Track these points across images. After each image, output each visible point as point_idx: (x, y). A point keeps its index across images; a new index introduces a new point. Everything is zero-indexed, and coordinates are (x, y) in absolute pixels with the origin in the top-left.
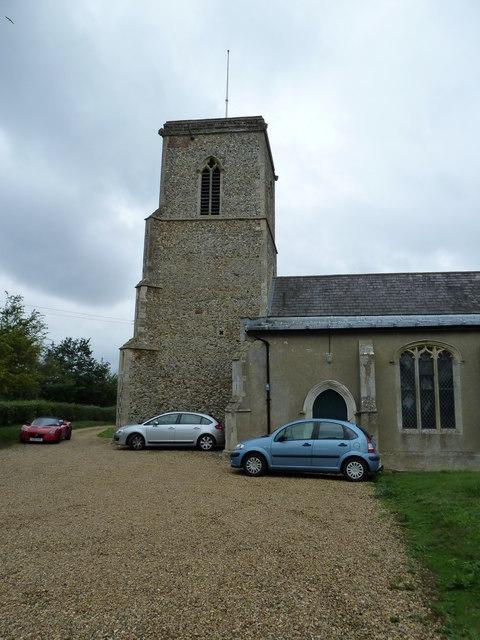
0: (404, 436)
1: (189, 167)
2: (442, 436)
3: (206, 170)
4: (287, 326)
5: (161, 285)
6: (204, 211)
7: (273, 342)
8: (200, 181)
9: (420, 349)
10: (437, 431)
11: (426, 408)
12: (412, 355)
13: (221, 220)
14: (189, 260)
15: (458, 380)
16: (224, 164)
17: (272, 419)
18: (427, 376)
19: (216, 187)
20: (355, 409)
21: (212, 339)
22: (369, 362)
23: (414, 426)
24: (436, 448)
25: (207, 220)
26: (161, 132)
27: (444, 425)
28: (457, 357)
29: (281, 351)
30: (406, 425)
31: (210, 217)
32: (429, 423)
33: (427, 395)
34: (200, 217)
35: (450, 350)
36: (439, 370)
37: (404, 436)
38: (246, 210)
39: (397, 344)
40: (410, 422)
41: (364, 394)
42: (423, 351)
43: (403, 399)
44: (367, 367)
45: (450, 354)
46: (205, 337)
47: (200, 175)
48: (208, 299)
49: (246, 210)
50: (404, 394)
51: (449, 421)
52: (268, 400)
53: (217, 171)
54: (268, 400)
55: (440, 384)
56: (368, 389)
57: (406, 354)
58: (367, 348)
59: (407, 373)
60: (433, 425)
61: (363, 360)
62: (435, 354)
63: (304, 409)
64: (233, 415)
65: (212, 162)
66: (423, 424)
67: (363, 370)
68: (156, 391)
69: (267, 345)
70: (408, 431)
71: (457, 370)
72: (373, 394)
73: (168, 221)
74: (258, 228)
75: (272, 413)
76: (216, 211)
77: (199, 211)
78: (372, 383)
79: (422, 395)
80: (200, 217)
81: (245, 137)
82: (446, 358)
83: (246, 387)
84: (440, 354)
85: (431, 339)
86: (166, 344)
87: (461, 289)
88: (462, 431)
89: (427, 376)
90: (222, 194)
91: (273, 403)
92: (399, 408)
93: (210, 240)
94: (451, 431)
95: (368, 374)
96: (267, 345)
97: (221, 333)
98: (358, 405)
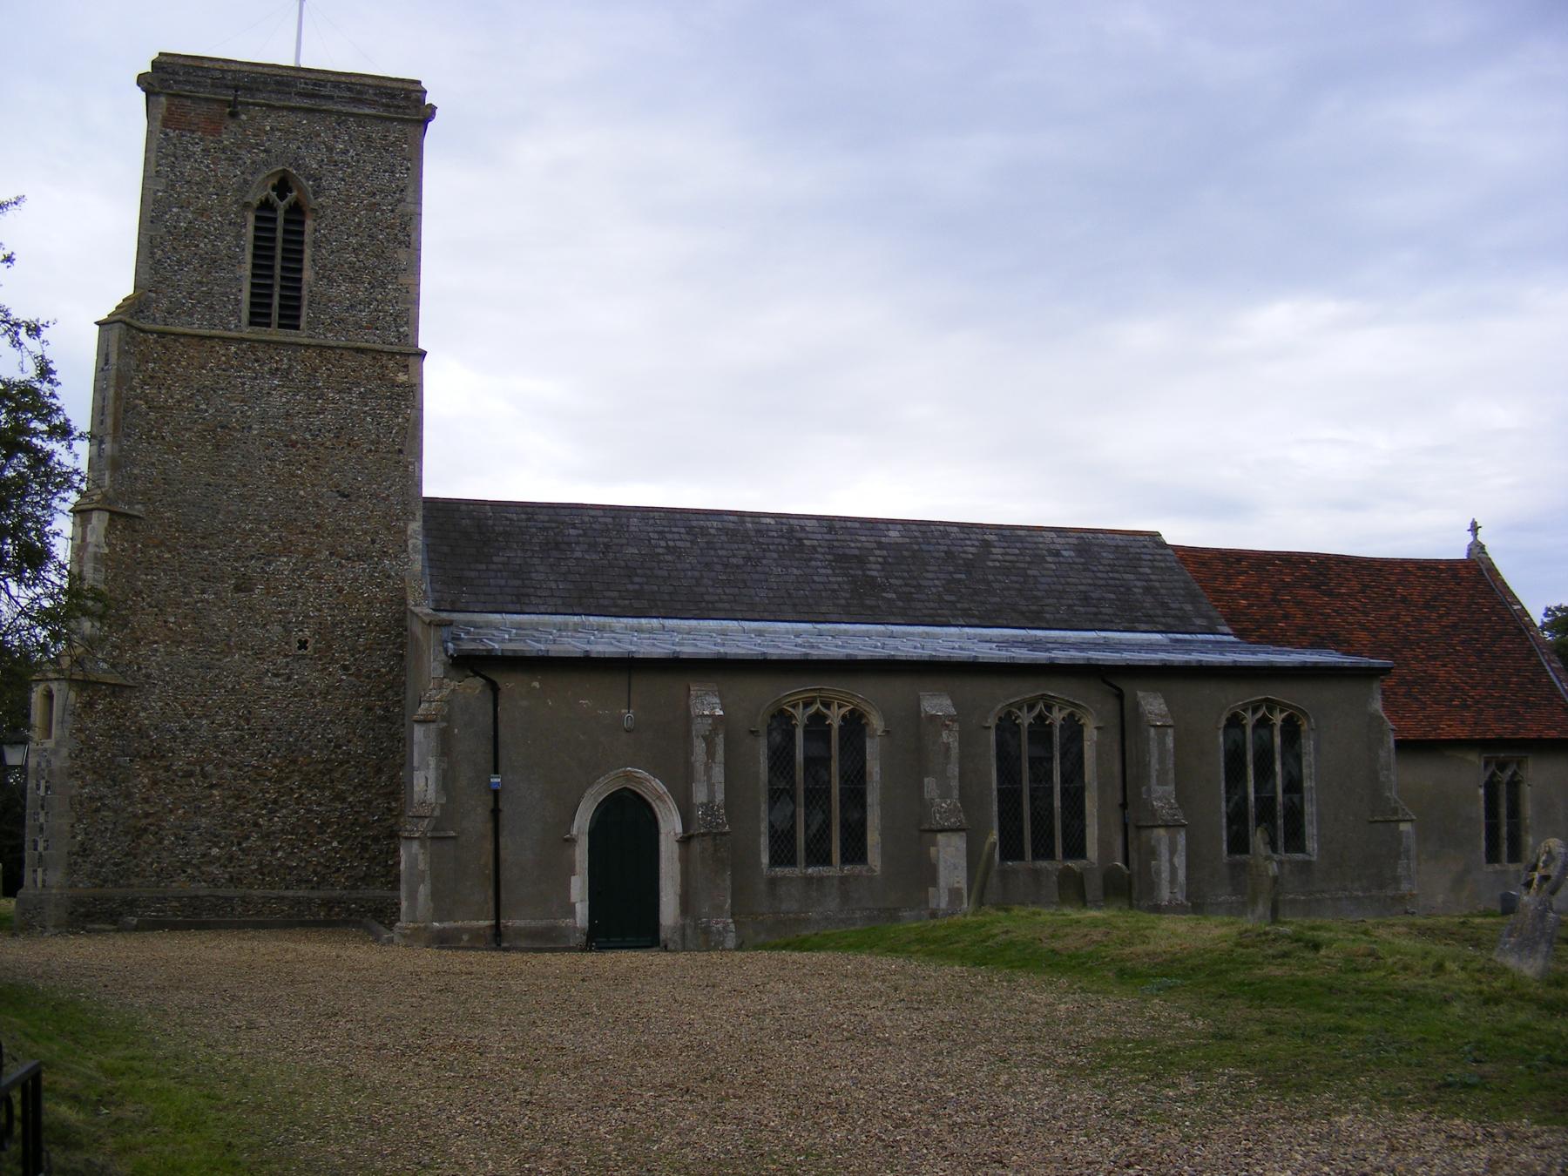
0: (773, 882)
1: (221, 191)
2: (844, 880)
3: (266, 205)
4: (534, 647)
5: (138, 509)
6: (259, 316)
7: (509, 683)
8: (249, 231)
9: (807, 705)
10: (835, 870)
11: (814, 828)
12: (792, 716)
13: (308, 346)
14: (217, 447)
15: (874, 767)
16: (316, 194)
17: (503, 853)
18: (817, 763)
19: (294, 255)
20: (679, 829)
21: (281, 660)
22: (714, 731)
23: (792, 862)
24: (832, 904)
25: (268, 343)
26: (142, 80)
27: (846, 860)
28: (876, 723)
29: (524, 703)
30: (775, 861)
31: (275, 334)
32: (819, 856)
33: (817, 796)
34: (248, 332)
35: (864, 707)
36: (841, 749)
37: (1004, 874)
38: (372, 325)
39: (762, 694)
40: (782, 852)
41: (700, 795)
42: (812, 710)
43: (771, 809)
44: (709, 741)
45: (862, 716)
46: (259, 655)
47: (251, 218)
48: (269, 556)
49: (372, 325)
50: (775, 796)
51: (855, 851)
52: (496, 812)
53: (297, 213)
54: (496, 812)
55: (841, 777)
56: (709, 787)
57: (782, 718)
58: (708, 704)
59: (781, 759)
60: (826, 860)
61: (700, 728)
62: (835, 717)
63: (574, 831)
64: (423, 846)
65: (283, 185)
66: (843, 855)
67: (700, 747)
68: (129, 796)
69: (494, 688)
70: (779, 871)
71: (872, 748)
72: (720, 797)
73: (162, 334)
74: (402, 378)
75: (504, 840)
76: (290, 319)
77: (245, 315)
78: (718, 773)
79: (806, 798)
80: (248, 332)
81: (376, 131)
82: (855, 724)
83: (447, 781)
84: (844, 717)
85: (829, 686)
86: (155, 673)
87: (861, 560)
88: (878, 869)
89: (817, 763)
90: (308, 275)
91: (504, 817)
92: (764, 827)
93: (277, 399)
94: (858, 868)
95: (710, 753)
96: (494, 688)
97: (303, 645)
98: (686, 821)
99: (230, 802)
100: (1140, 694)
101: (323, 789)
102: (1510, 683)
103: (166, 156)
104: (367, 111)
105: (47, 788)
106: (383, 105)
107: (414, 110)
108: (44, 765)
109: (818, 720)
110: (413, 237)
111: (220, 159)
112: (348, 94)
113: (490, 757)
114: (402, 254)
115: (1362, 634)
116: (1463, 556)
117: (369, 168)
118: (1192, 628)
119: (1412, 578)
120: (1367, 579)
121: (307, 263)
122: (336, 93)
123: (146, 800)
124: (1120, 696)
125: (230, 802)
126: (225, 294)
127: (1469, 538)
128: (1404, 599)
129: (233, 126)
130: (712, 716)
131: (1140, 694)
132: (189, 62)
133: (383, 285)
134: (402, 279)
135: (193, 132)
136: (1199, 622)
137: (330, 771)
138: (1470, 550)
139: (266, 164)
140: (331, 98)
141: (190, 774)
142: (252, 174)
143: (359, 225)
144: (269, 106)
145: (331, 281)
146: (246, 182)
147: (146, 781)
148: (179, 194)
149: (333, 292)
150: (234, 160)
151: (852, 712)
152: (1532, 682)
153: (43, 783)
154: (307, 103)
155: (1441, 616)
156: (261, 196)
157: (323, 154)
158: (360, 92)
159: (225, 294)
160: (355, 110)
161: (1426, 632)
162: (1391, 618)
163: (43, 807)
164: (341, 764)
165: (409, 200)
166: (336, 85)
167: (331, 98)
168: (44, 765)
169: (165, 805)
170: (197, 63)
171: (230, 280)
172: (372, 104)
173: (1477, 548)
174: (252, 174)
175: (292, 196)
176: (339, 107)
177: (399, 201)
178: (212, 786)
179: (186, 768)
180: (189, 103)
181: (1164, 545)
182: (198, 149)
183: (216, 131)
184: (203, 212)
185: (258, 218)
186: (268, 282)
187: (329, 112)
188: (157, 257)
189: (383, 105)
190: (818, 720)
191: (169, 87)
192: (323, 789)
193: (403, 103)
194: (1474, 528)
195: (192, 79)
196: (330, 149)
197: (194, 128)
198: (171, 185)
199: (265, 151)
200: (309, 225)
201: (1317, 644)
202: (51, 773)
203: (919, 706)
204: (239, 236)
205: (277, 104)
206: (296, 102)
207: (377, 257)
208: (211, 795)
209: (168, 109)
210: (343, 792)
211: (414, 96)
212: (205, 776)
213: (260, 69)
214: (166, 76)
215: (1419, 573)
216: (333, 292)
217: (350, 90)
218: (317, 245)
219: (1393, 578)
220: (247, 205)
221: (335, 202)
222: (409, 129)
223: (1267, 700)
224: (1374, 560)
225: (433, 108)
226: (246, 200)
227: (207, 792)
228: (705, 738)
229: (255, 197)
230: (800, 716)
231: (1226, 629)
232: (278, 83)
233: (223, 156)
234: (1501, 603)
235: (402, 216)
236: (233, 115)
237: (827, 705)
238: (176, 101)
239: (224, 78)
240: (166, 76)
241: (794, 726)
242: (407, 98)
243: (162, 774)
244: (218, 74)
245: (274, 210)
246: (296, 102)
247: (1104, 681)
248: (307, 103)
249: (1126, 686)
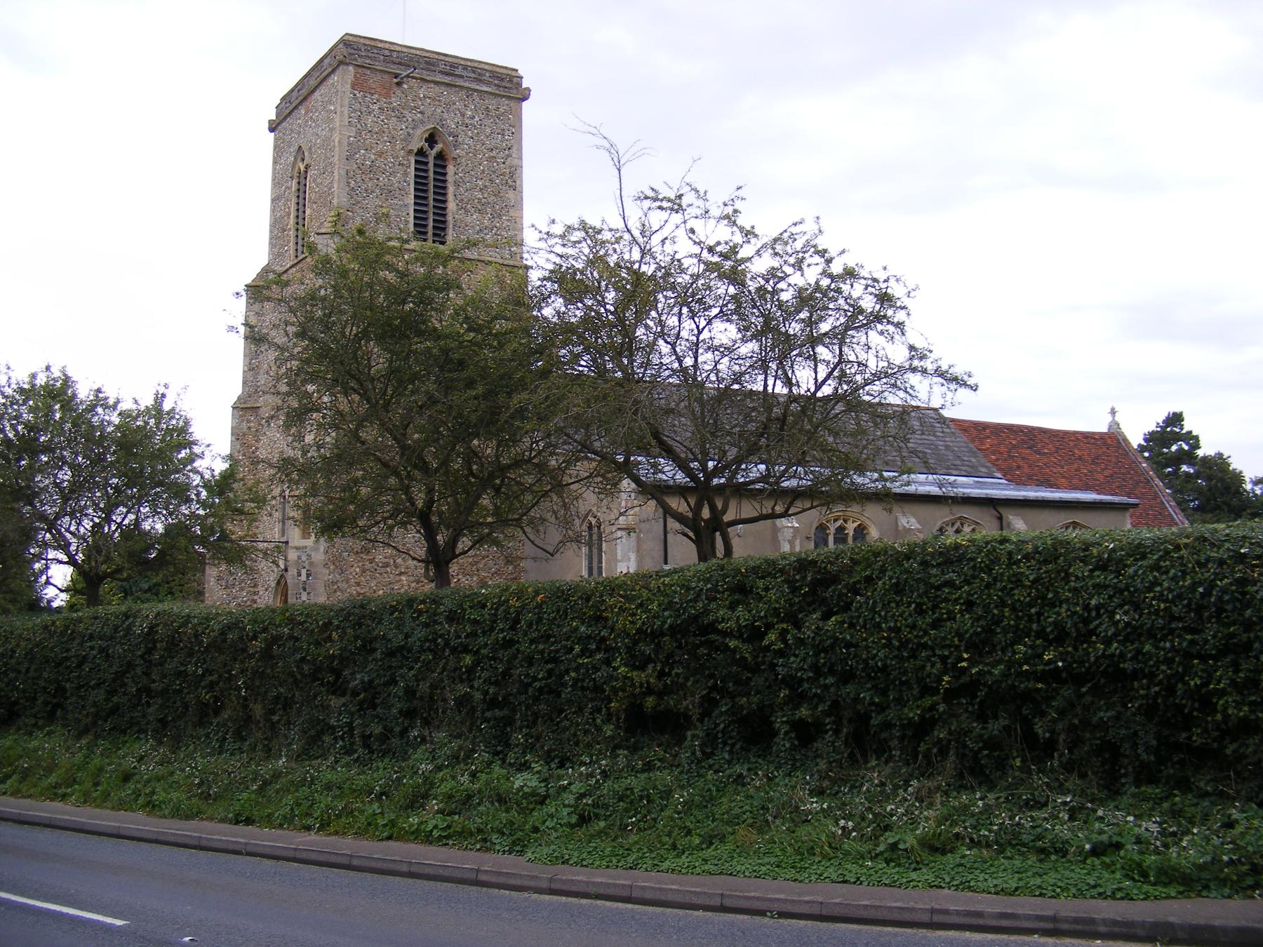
1: (392, 140)
3: (421, 152)
22: (794, 537)
35: (868, 522)
45: (865, 528)
62: (851, 527)
65: (432, 139)
81: (492, 103)
90: (451, 205)
99: (413, 585)
100: (1011, 517)
101: (472, 576)
102: (1148, 514)
103: (355, 111)
104: (485, 89)
105: (308, 575)
106: (495, 85)
107: (515, 91)
108: (304, 558)
109: (841, 529)
110: (518, 183)
111: (391, 117)
112: (473, 75)
113: (662, 553)
114: (511, 195)
115: (1063, 480)
116: (1105, 430)
117: (488, 130)
118: (981, 474)
119: (1082, 444)
120: (1058, 444)
121: (450, 197)
122: (465, 73)
123: (358, 584)
124: (1000, 518)
125: (413, 585)
126: (397, 216)
127: (1110, 418)
128: (1080, 458)
129: (398, 92)
130: (793, 527)
131: (1011, 517)
132: (368, 42)
133: (500, 216)
134: (511, 213)
135: (372, 94)
136: (983, 470)
137: (476, 563)
138: (1110, 426)
139: (422, 122)
140: (462, 77)
141: (386, 565)
142: (413, 129)
143: (483, 171)
144: (423, 80)
145: (467, 211)
146: (409, 134)
147: (358, 570)
148: (365, 140)
149: (469, 219)
150: (400, 118)
151: (859, 525)
152: (1160, 514)
153: (304, 572)
154: (447, 79)
155: (1103, 470)
156: (419, 146)
157: (458, 119)
158: (480, 74)
159: (397, 216)
160: (478, 87)
161: (1096, 480)
162: (1076, 470)
163: (305, 590)
164: (483, 558)
165: (514, 156)
166: (465, 68)
167: (462, 77)
168: (304, 558)
169: (371, 587)
170: (372, 43)
171: (401, 206)
172: (489, 84)
173: (1115, 425)
174: (413, 129)
175: (438, 147)
176: (467, 84)
177: (509, 156)
178: (401, 574)
179: (385, 560)
180: (368, 72)
181: (944, 421)
182: (376, 107)
183: (387, 96)
184: (380, 154)
185: (417, 162)
186: (425, 209)
187: (461, 87)
188: (352, 185)
189: (495, 85)
190: (841, 529)
191: (355, 59)
192: (472, 576)
193: (508, 85)
194: (1113, 412)
195: (370, 55)
196: (463, 115)
197: (373, 91)
198: (359, 133)
199: (420, 113)
200: (451, 169)
201: (1086, 488)
202: (311, 564)
203: (897, 522)
204: (406, 174)
205: (428, 78)
206: (439, 78)
207: (495, 195)
208: (401, 580)
209: (355, 76)
210: (485, 577)
211: (515, 80)
212: (396, 566)
213: (414, 51)
214: (353, 51)
215: (1085, 441)
216: (469, 219)
217: (474, 72)
218: (457, 184)
219: (1071, 443)
220: (410, 152)
221: (467, 154)
222: (512, 104)
223: (1074, 522)
224: (1058, 431)
225: (528, 90)
226: (410, 148)
227: (398, 578)
228: (789, 541)
229: (416, 145)
230: (832, 529)
231: (999, 475)
232: (426, 63)
233: (393, 114)
234: (1134, 462)
235: (511, 167)
236: (399, 84)
237: (845, 521)
238: (360, 71)
239: (391, 56)
240: (353, 51)
241: (828, 535)
242: (511, 81)
243: (368, 565)
244: (387, 53)
245: (426, 156)
246: (439, 78)
247: (995, 509)
248: (447, 79)
249: (1004, 511)
